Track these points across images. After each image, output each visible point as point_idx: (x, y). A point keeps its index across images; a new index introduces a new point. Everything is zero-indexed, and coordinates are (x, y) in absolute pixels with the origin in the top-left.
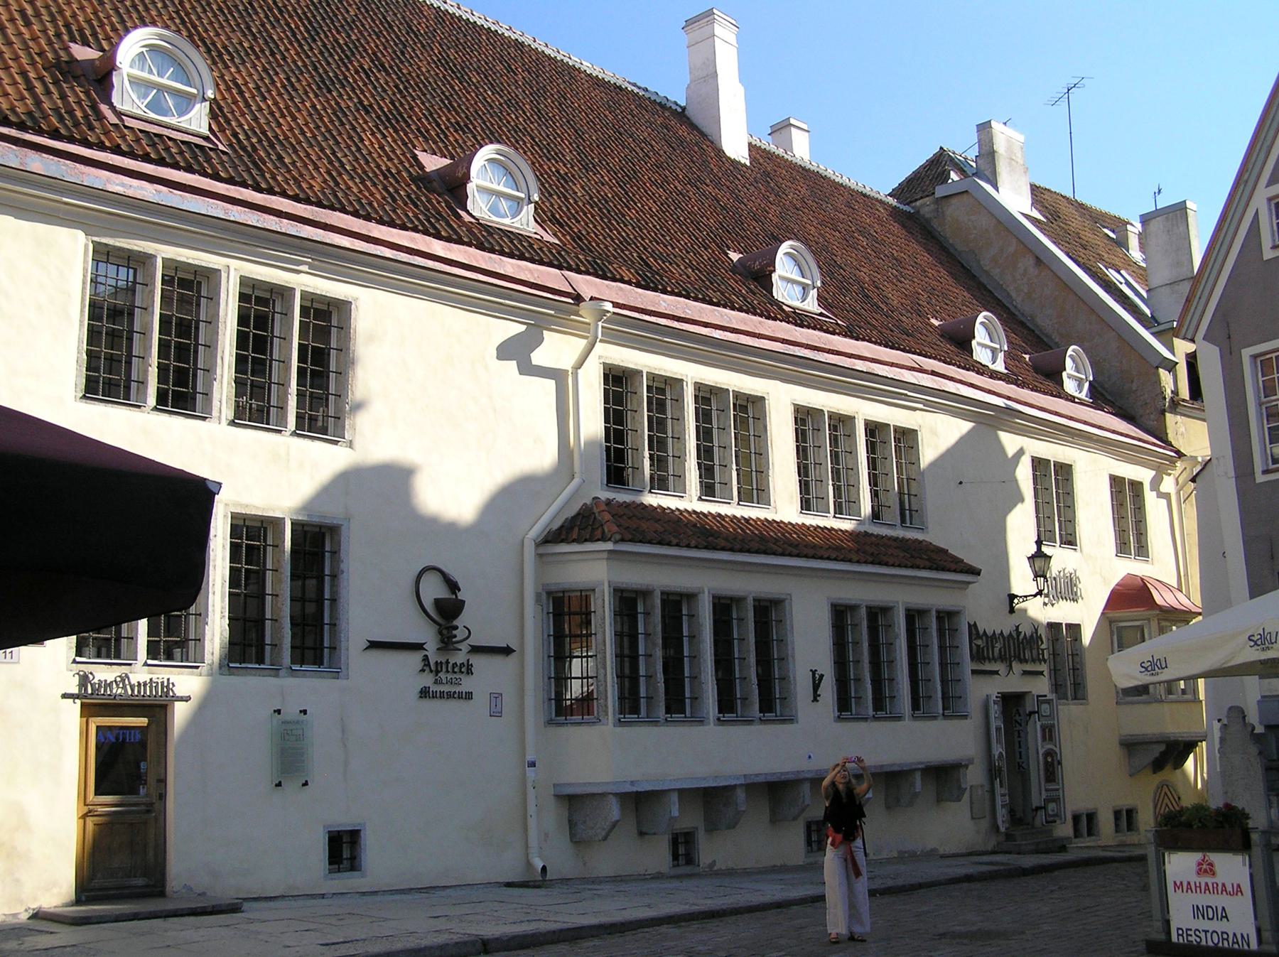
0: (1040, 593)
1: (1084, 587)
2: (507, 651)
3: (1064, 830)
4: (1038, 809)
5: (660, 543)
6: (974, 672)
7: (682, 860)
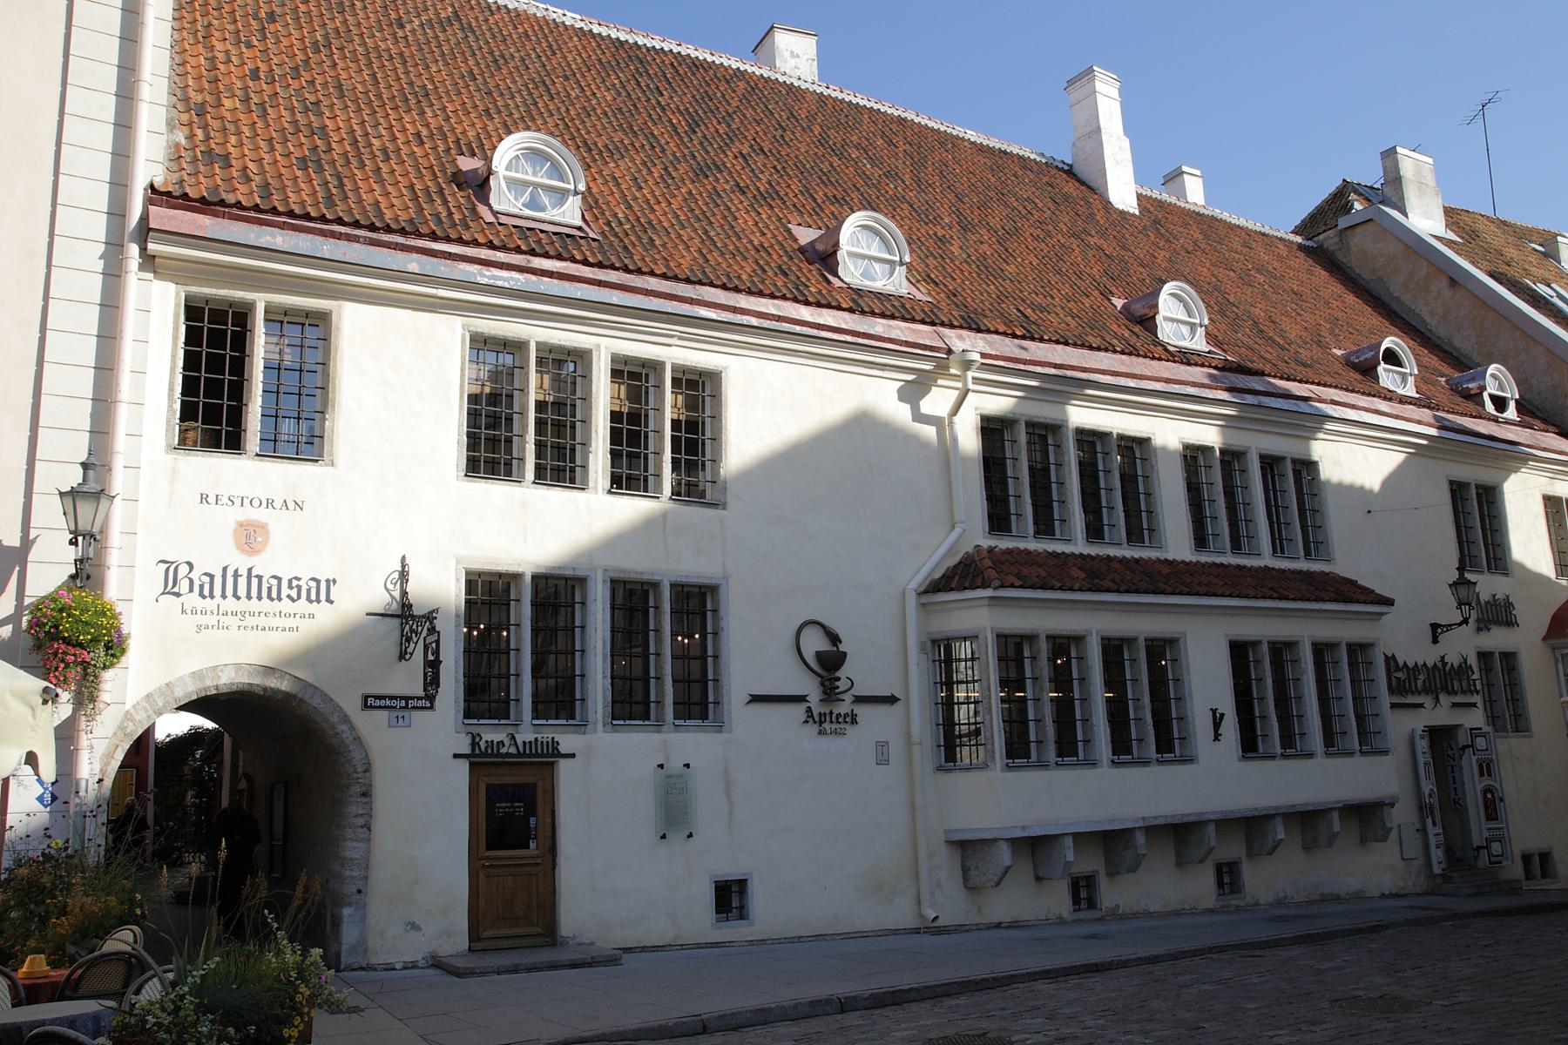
0: (1465, 621)
1: (1520, 612)
2: (891, 700)
3: (1516, 870)
4: (1479, 848)
5: (1043, 587)
6: (1393, 706)
7: (1084, 905)
